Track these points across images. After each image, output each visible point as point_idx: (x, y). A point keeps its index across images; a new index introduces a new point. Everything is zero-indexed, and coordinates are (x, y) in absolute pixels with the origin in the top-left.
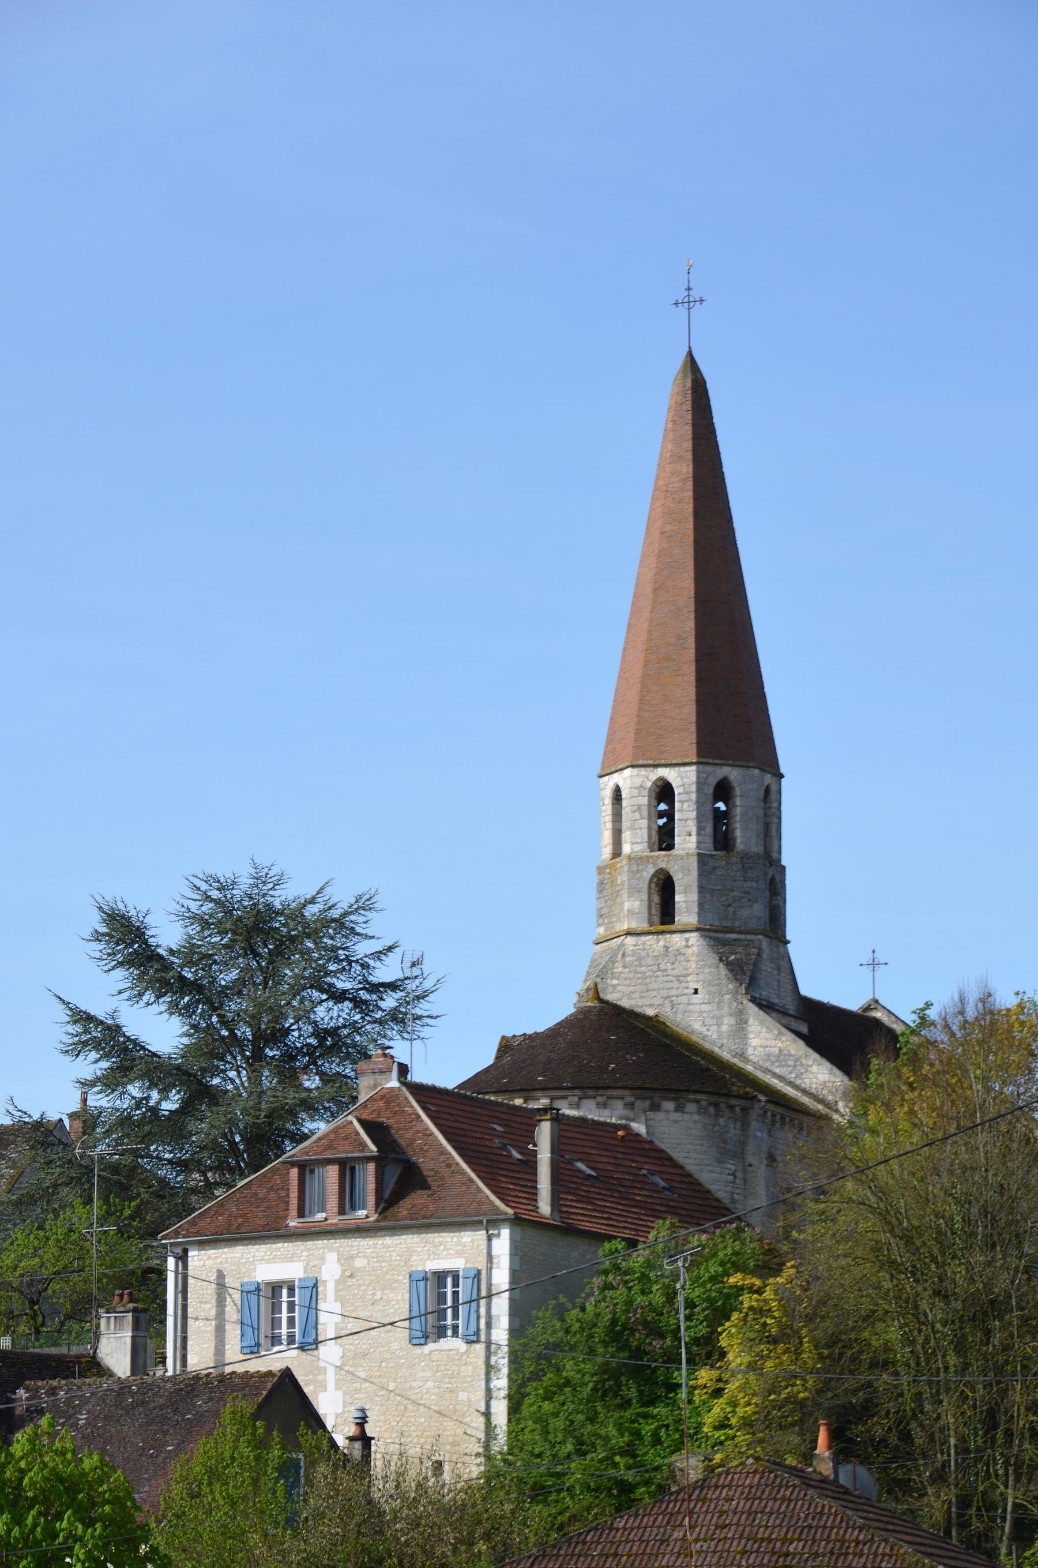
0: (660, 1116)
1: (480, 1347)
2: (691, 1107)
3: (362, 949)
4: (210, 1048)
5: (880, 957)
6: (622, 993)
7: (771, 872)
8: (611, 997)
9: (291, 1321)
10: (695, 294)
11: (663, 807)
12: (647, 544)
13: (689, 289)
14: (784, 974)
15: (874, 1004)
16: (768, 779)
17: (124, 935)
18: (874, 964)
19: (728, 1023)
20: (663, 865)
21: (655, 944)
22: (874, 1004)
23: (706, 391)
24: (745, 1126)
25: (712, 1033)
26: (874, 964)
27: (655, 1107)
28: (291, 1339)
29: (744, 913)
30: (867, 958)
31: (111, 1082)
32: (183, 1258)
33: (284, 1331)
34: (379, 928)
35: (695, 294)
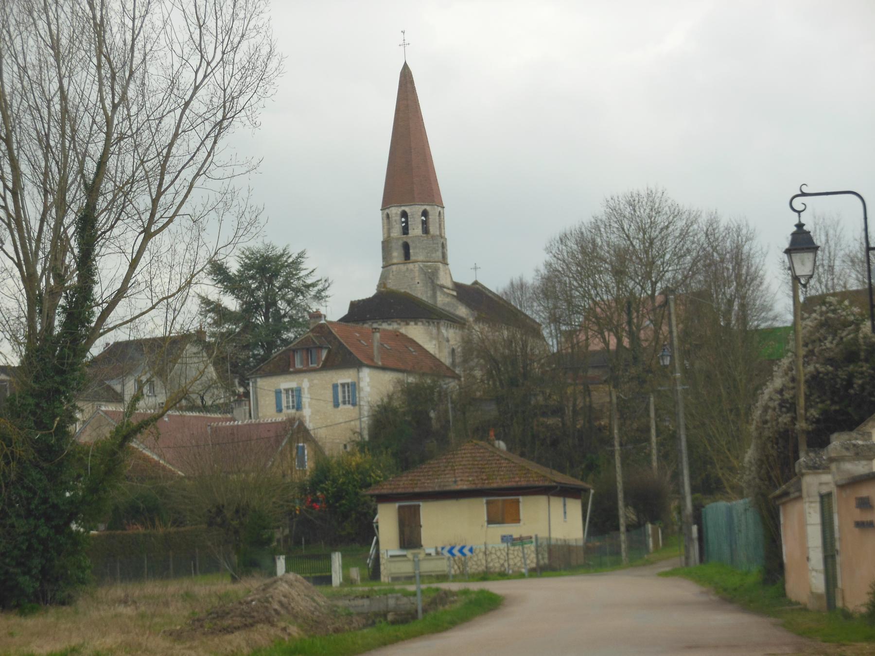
0: (409, 327)
1: (357, 408)
2: (420, 323)
3: (302, 273)
4: (249, 309)
5: (478, 266)
6: (392, 285)
7: (442, 240)
8: (389, 286)
9: (293, 402)
10: (406, 42)
11: (403, 220)
12: (567, 578)
13: (404, 44)
14: (448, 276)
15: (476, 283)
16: (440, 209)
17: (218, 270)
18: (476, 268)
19: (430, 293)
20: (405, 240)
21: (403, 268)
22: (476, 283)
23: (412, 82)
24: (438, 329)
25: (424, 298)
26: (476, 268)
27: (407, 324)
28: (293, 407)
29: (434, 255)
30: (473, 266)
31: (217, 323)
32: (255, 382)
33: (291, 404)
34: (307, 265)
35: (406, 42)
